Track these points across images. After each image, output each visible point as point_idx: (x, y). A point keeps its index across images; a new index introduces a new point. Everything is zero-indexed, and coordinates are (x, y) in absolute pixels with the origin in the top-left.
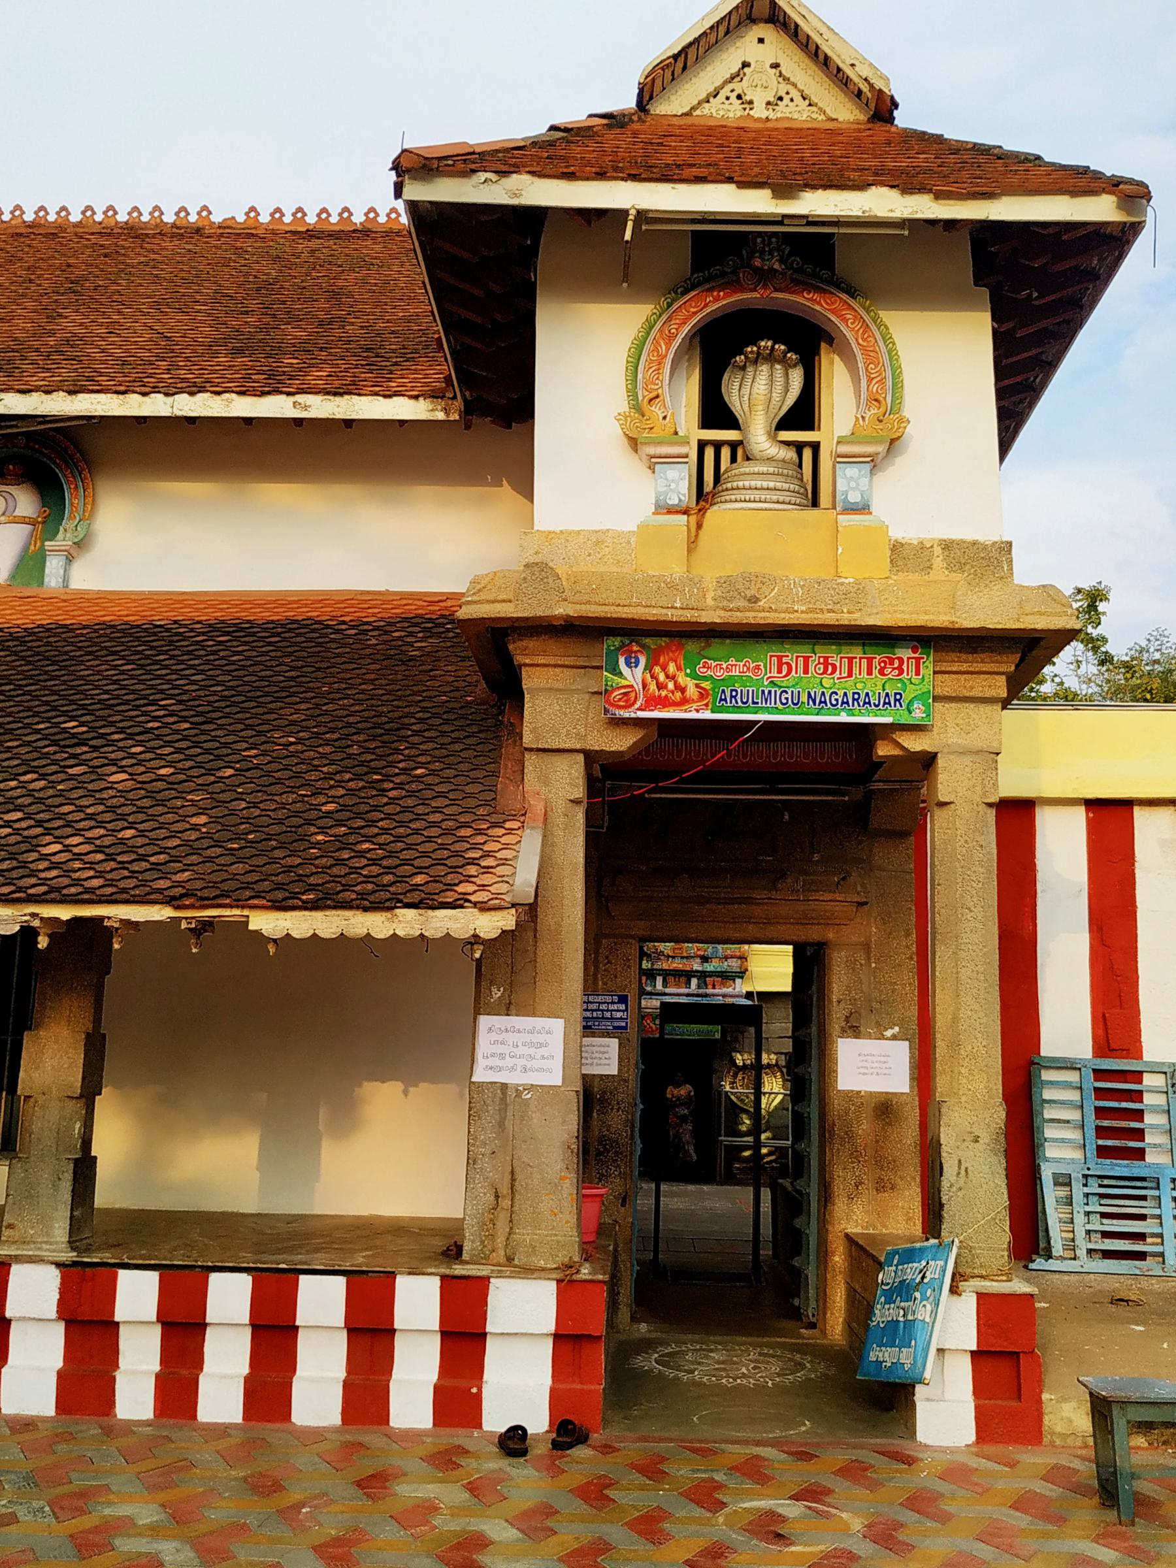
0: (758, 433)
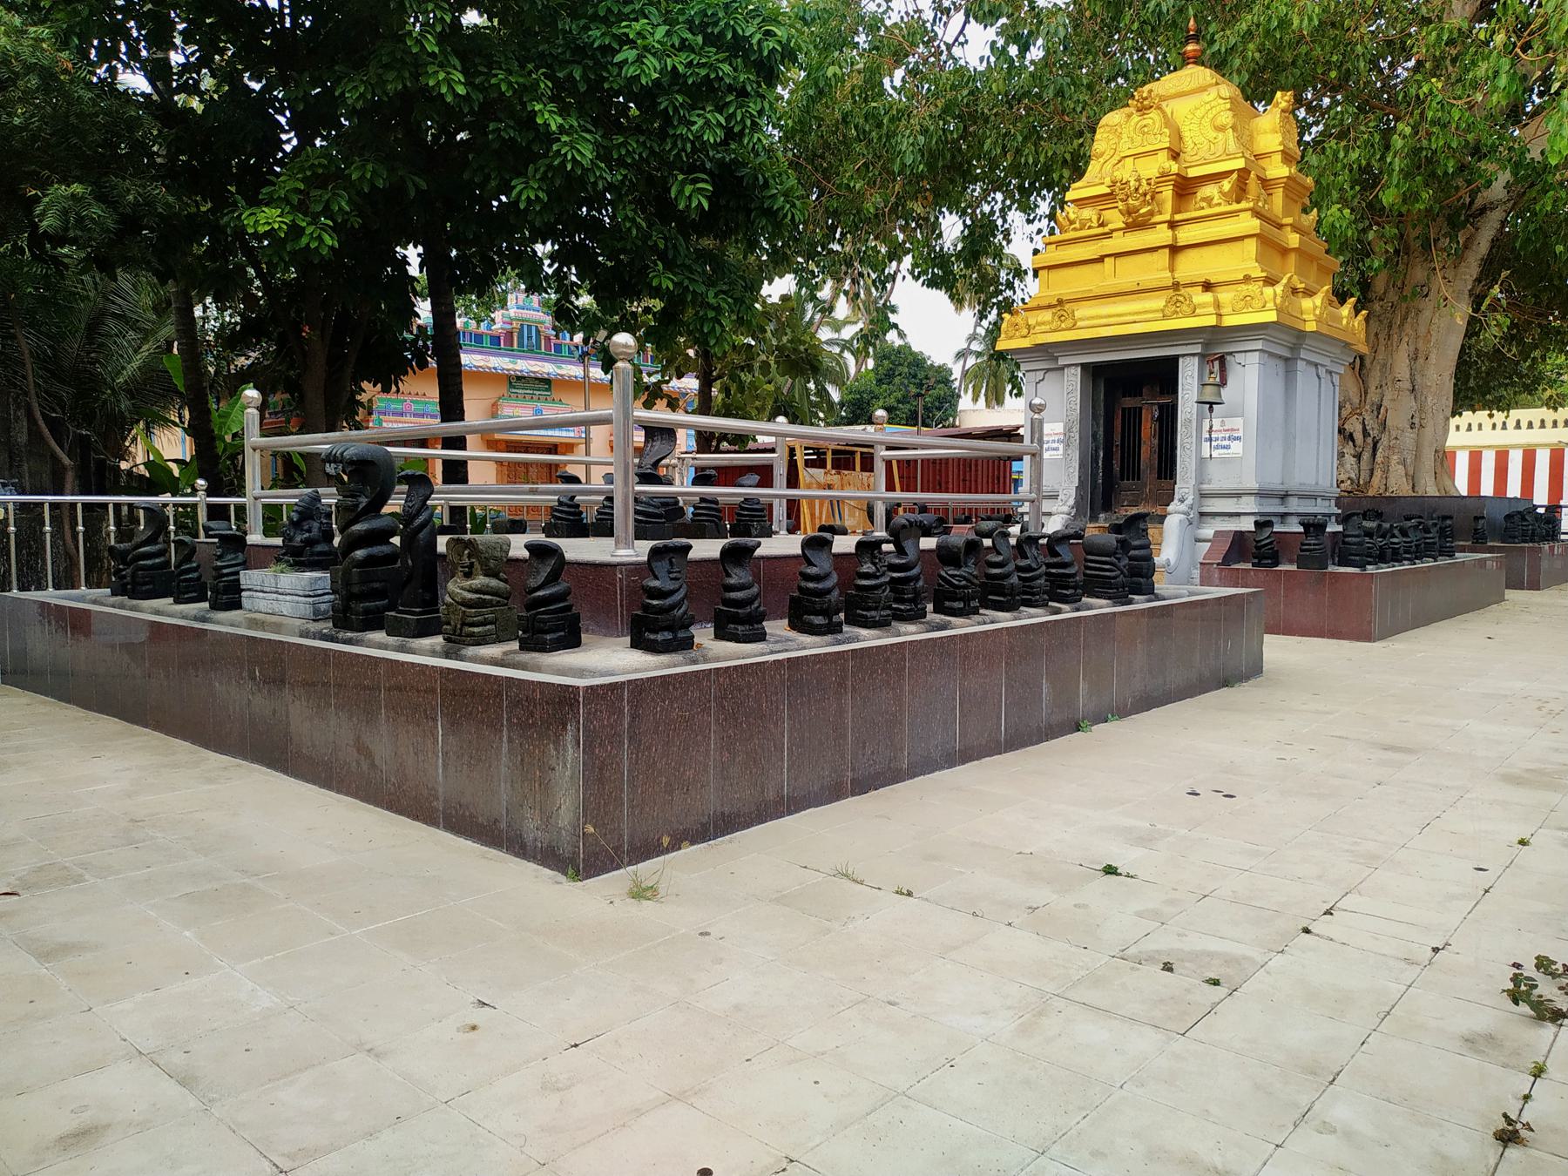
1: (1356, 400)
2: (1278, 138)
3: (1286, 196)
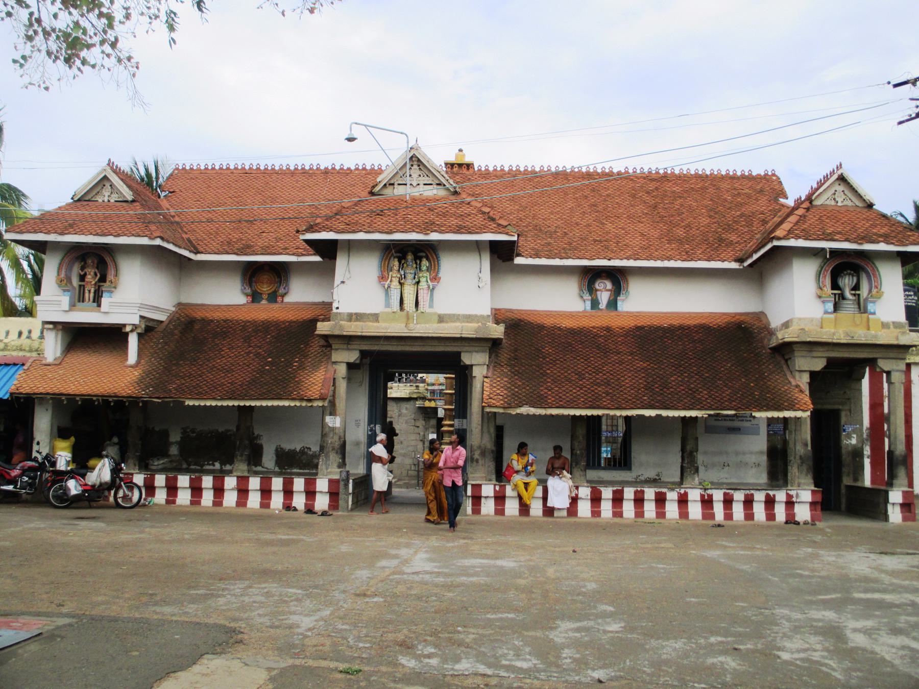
0: (848, 294)
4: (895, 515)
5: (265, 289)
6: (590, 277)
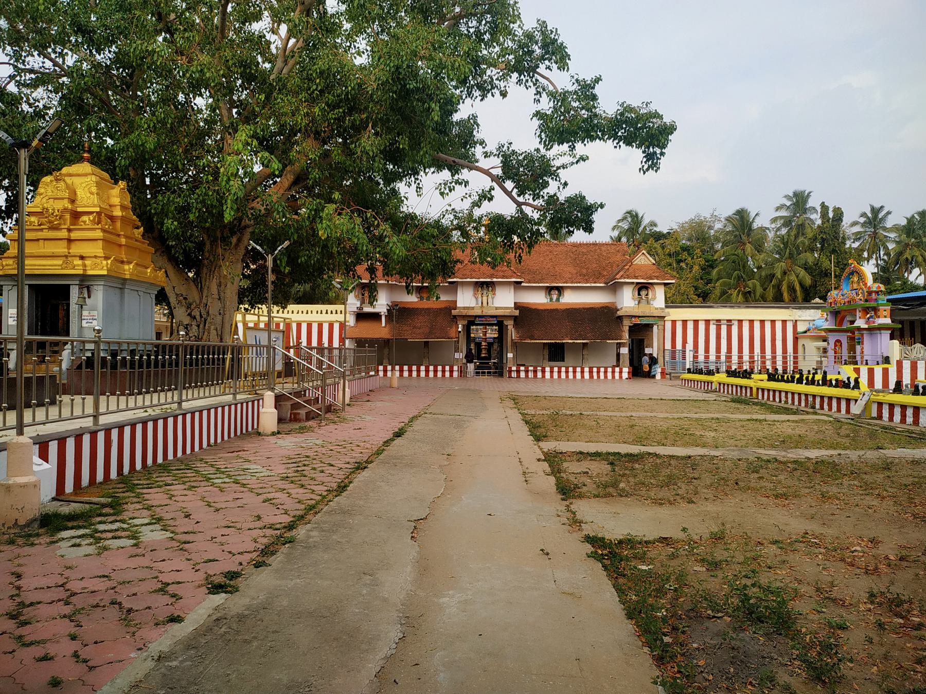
1: (198, 302)
2: (118, 200)
3: (122, 223)
4: (658, 377)
5: (425, 295)
6: (549, 290)
